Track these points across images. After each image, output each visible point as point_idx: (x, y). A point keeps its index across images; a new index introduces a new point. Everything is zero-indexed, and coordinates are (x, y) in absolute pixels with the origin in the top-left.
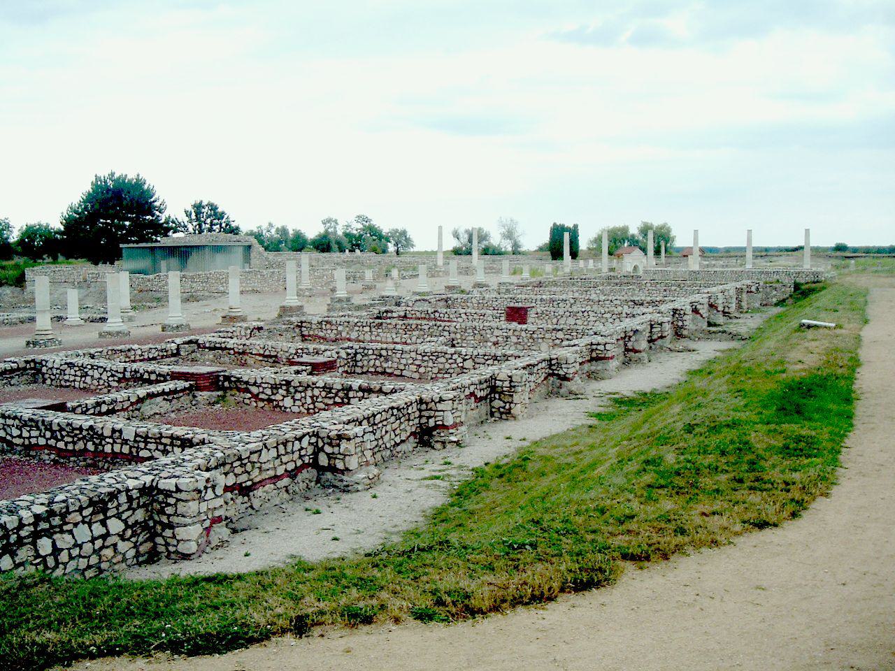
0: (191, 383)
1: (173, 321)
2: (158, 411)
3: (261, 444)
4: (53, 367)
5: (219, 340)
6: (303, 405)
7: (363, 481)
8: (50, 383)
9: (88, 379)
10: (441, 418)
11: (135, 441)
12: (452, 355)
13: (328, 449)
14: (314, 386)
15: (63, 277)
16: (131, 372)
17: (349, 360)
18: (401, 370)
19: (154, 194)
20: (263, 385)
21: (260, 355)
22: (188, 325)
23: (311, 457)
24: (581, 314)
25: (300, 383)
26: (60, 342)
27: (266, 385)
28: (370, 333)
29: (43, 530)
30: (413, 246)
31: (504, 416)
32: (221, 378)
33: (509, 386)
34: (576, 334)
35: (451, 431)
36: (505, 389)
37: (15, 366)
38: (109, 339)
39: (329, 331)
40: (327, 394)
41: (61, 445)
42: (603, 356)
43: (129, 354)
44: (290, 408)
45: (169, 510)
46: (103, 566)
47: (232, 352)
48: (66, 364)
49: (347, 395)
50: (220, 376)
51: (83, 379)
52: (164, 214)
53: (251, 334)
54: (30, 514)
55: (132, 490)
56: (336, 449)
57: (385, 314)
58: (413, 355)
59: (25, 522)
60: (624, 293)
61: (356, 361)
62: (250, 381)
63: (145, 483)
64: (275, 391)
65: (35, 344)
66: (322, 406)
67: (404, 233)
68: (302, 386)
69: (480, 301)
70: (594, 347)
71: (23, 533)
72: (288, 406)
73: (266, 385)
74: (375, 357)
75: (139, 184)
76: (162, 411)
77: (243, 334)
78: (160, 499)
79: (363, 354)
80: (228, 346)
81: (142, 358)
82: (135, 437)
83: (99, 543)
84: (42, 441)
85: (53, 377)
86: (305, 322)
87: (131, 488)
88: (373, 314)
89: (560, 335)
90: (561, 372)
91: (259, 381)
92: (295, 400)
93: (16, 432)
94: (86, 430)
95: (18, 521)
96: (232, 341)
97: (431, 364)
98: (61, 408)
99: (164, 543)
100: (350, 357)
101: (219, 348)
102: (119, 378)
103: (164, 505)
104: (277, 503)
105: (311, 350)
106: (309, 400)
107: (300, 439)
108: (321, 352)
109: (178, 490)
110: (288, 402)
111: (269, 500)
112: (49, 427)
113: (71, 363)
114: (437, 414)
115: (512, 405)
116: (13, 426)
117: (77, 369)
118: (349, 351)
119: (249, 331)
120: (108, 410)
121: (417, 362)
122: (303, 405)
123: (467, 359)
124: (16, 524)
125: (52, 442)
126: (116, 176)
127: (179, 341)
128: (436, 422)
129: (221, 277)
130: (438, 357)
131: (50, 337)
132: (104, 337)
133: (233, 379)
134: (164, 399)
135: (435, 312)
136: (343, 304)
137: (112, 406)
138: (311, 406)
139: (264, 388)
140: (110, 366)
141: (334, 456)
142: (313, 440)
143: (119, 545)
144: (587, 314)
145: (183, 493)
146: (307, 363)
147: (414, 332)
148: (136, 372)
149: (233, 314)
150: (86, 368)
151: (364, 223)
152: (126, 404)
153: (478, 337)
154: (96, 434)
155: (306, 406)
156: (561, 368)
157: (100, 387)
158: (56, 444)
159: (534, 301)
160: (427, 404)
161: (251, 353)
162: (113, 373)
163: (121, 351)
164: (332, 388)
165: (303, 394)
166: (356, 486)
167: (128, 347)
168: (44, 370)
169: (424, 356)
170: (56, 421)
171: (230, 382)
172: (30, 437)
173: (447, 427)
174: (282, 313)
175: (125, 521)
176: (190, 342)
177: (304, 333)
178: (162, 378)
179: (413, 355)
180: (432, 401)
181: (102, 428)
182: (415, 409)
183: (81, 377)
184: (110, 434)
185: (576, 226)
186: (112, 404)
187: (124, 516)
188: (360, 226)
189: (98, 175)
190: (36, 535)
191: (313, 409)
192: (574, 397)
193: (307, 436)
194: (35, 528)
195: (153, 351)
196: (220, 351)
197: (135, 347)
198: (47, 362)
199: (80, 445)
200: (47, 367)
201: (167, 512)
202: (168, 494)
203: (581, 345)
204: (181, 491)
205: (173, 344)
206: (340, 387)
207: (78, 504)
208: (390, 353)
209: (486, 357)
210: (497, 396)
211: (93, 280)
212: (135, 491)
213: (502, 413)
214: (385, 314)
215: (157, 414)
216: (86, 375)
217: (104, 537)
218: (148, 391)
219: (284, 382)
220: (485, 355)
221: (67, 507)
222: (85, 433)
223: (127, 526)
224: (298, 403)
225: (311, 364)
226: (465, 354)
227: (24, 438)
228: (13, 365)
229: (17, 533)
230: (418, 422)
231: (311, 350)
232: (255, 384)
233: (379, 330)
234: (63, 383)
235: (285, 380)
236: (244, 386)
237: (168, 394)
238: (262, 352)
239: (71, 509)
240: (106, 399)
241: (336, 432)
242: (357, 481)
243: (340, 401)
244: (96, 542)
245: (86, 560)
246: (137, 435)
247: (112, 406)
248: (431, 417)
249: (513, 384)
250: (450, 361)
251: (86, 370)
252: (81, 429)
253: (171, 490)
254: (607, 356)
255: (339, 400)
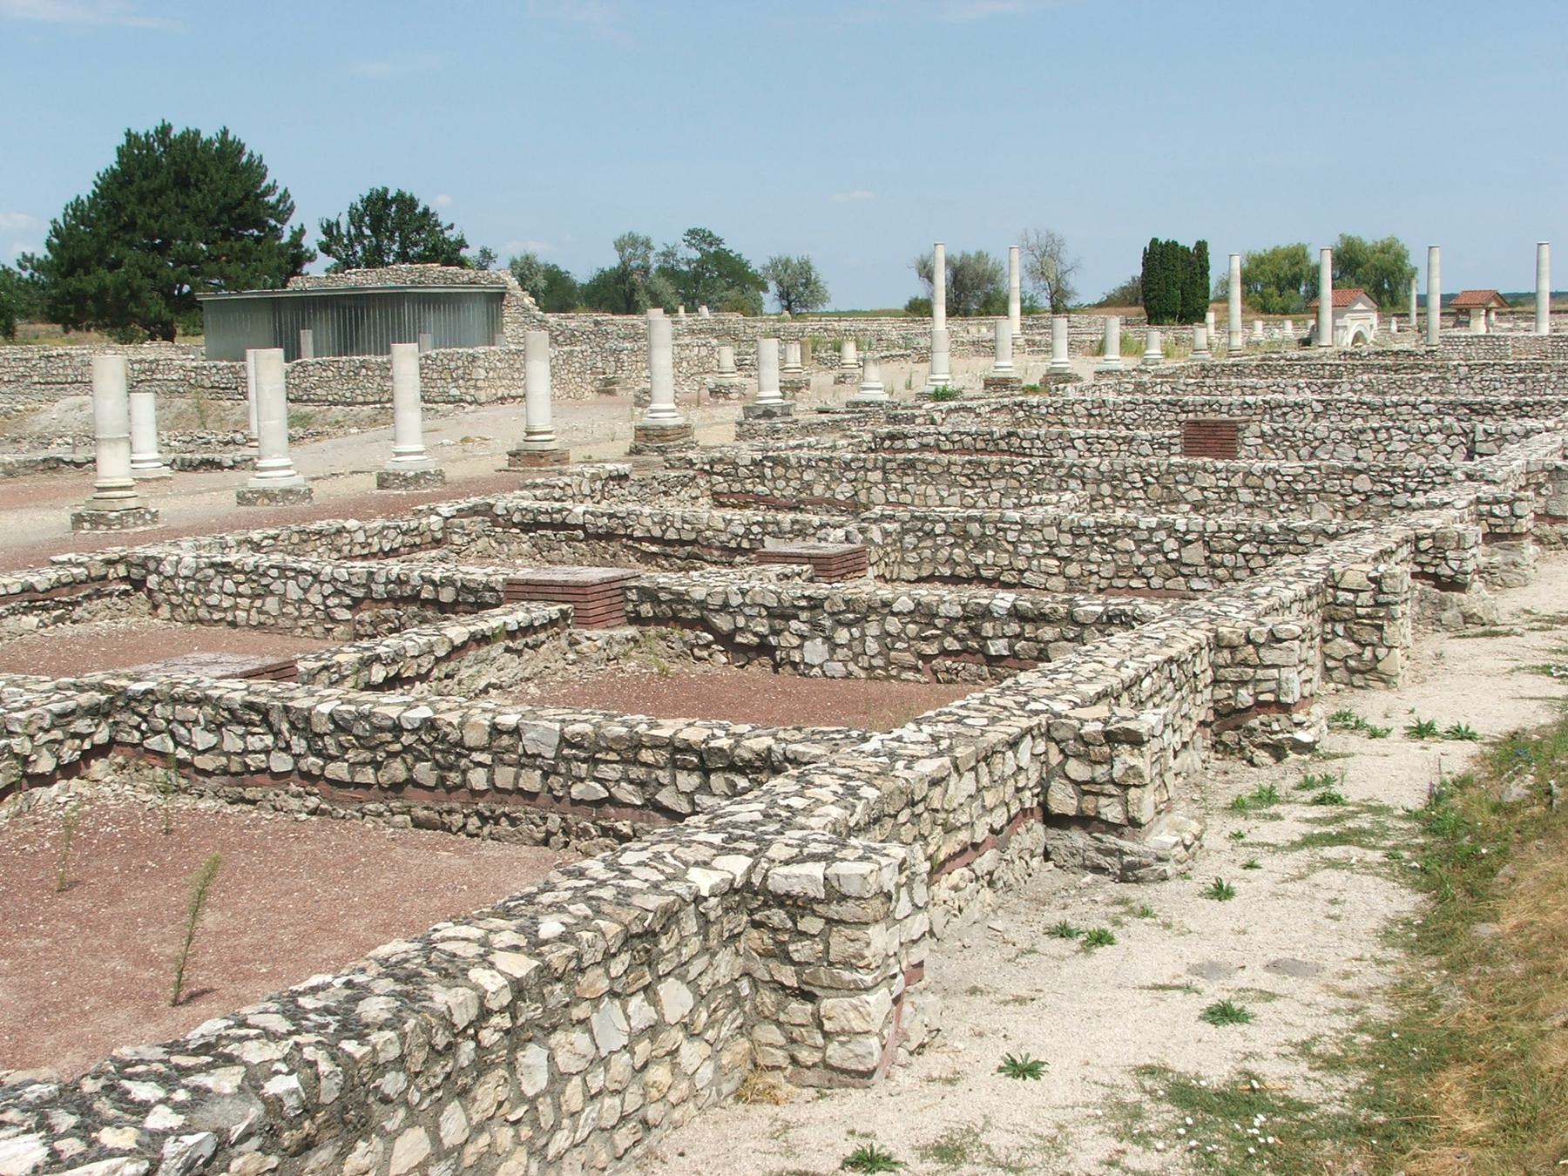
0: (565, 607)
1: (409, 466)
2: (494, 681)
3: (946, 760)
4: (177, 575)
5: (545, 505)
6: (855, 659)
7: (1174, 852)
8: (168, 615)
9: (271, 604)
10: (1273, 685)
11: (559, 756)
12: (1151, 530)
13: (1076, 770)
14: (886, 611)
15: (70, 371)
16: (389, 581)
17: (889, 549)
18: (1021, 572)
19: (263, 176)
20: (747, 610)
21: (653, 540)
22: (440, 473)
23: (1036, 791)
24: (1370, 436)
25: (847, 602)
26: (155, 515)
27: (755, 611)
28: (882, 487)
29: (531, 1023)
30: (822, 301)
31: (1358, 680)
32: (633, 595)
33: (1372, 602)
34: (1401, 480)
35: (1297, 717)
36: (1360, 611)
37: (80, 572)
38: (263, 508)
39: (781, 484)
40: (922, 631)
41: (337, 770)
42: (1506, 530)
43: (339, 542)
44: (821, 666)
45: (801, 950)
46: (653, 1113)
47: (580, 534)
48: (212, 565)
49: (975, 632)
50: (630, 589)
51: (258, 603)
52: (289, 223)
53: (602, 491)
54: (502, 981)
55: (706, 899)
56: (1100, 771)
57: (887, 443)
58: (1051, 533)
59: (494, 1005)
60: (1420, 389)
61: (903, 550)
62: (709, 600)
63: (734, 879)
64: (778, 624)
65: (97, 520)
66: (909, 658)
67: (805, 269)
68: (854, 611)
69: (1095, 412)
70: (1484, 508)
71: (488, 1037)
72: (817, 661)
73: (755, 611)
74: (951, 540)
75: (228, 152)
76: (506, 679)
77: (587, 491)
78: (776, 921)
79: (920, 534)
80: (570, 520)
81: (365, 551)
82: (559, 749)
83: (643, 1049)
84: (281, 763)
85: (174, 599)
86: (721, 460)
87: (705, 893)
88: (860, 444)
89: (1363, 483)
90: (1444, 571)
91: (736, 600)
92: (834, 647)
93: (203, 739)
94: (414, 731)
95: (476, 1003)
96: (580, 509)
97: (1095, 556)
98: (281, 672)
99: (782, 1040)
100: (889, 540)
101: (545, 526)
102: (354, 599)
103: (786, 937)
104: (977, 916)
105: (786, 526)
106: (873, 646)
107: (1014, 745)
108: (812, 531)
109: (835, 895)
110: (815, 651)
111: (960, 910)
112: (302, 723)
113: (225, 565)
114: (1260, 674)
115: (1382, 652)
116: (196, 722)
117: (241, 578)
118: (889, 527)
119: (598, 485)
120: (386, 679)
121: (1062, 552)
122: (855, 659)
123: (1190, 542)
124: (473, 1012)
125: (312, 763)
126: (176, 132)
127: (445, 509)
128: (1257, 694)
129: (453, 365)
130: (1114, 537)
131: (132, 503)
132: (249, 502)
133: (663, 596)
134: (508, 650)
135: (1010, 434)
136: (775, 420)
137: (396, 668)
138: (878, 662)
139: (749, 618)
140: (328, 569)
141: (1096, 788)
142: (1041, 747)
143: (682, 1051)
144: (1385, 436)
145: (850, 903)
146: (800, 556)
147: (994, 483)
148: (400, 582)
149: (539, 447)
150: (265, 574)
151: (705, 247)
152: (426, 663)
153: (1155, 491)
154: (443, 739)
155: (864, 661)
156: (1445, 559)
157: (302, 623)
158: (323, 768)
159: (1224, 409)
160: (1233, 648)
161: (630, 537)
162: (339, 585)
163: (320, 533)
164: (936, 615)
165: (856, 632)
166: (1160, 867)
167: (336, 524)
168: (152, 581)
169: (1078, 536)
170: (325, 708)
171: (656, 601)
172: (246, 752)
173: (1285, 708)
174: (640, 444)
175: (693, 985)
176: (474, 511)
177: (718, 488)
178: (473, 600)
179: (1051, 533)
180: (1249, 641)
181: (462, 725)
182: (1206, 665)
183: (255, 596)
184: (485, 740)
185: (1201, 246)
186: (394, 661)
187: (694, 971)
188: (695, 254)
189: (133, 132)
190: (516, 1038)
191: (885, 669)
192: (1481, 629)
193: (1029, 737)
194: (514, 1018)
195: (392, 534)
196: (549, 533)
197: (352, 524)
198: (159, 561)
199: (397, 770)
200: (160, 574)
201: (796, 957)
202: (797, 905)
203: (1459, 504)
204: (844, 898)
205: (434, 518)
206: (956, 611)
207: (601, 945)
208: (990, 530)
209: (1240, 537)
210: (1340, 629)
211: (143, 377)
212: (713, 901)
213: (1352, 671)
214: (887, 443)
215: (493, 686)
216: (268, 591)
217: (653, 1031)
218: (472, 629)
219: (803, 603)
220: (1235, 533)
221: (579, 957)
222: (407, 739)
223: (701, 998)
224: (841, 653)
225: (810, 559)
226: (1183, 529)
227: (228, 754)
228: (75, 571)
229: (475, 1037)
230: (1209, 698)
231: (786, 526)
232: (725, 607)
233: (906, 480)
234: (203, 613)
235: (809, 598)
236: (697, 613)
237: (512, 635)
238: (657, 532)
239: (588, 959)
240: (380, 650)
241: (1099, 726)
242: (1161, 854)
243: (956, 646)
244: (636, 1049)
245: (617, 1100)
246: (565, 741)
247: (396, 668)
248: (1244, 683)
249: (1381, 598)
250: (1147, 547)
251: (264, 581)
252: (397, 729)
253: (811, 894)
254: (1516, 530)
255: (954, 645)
